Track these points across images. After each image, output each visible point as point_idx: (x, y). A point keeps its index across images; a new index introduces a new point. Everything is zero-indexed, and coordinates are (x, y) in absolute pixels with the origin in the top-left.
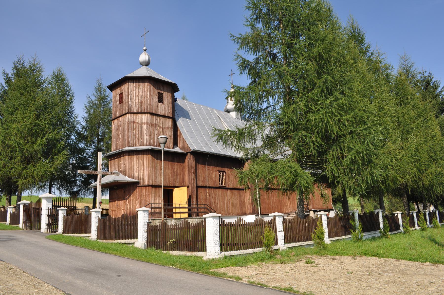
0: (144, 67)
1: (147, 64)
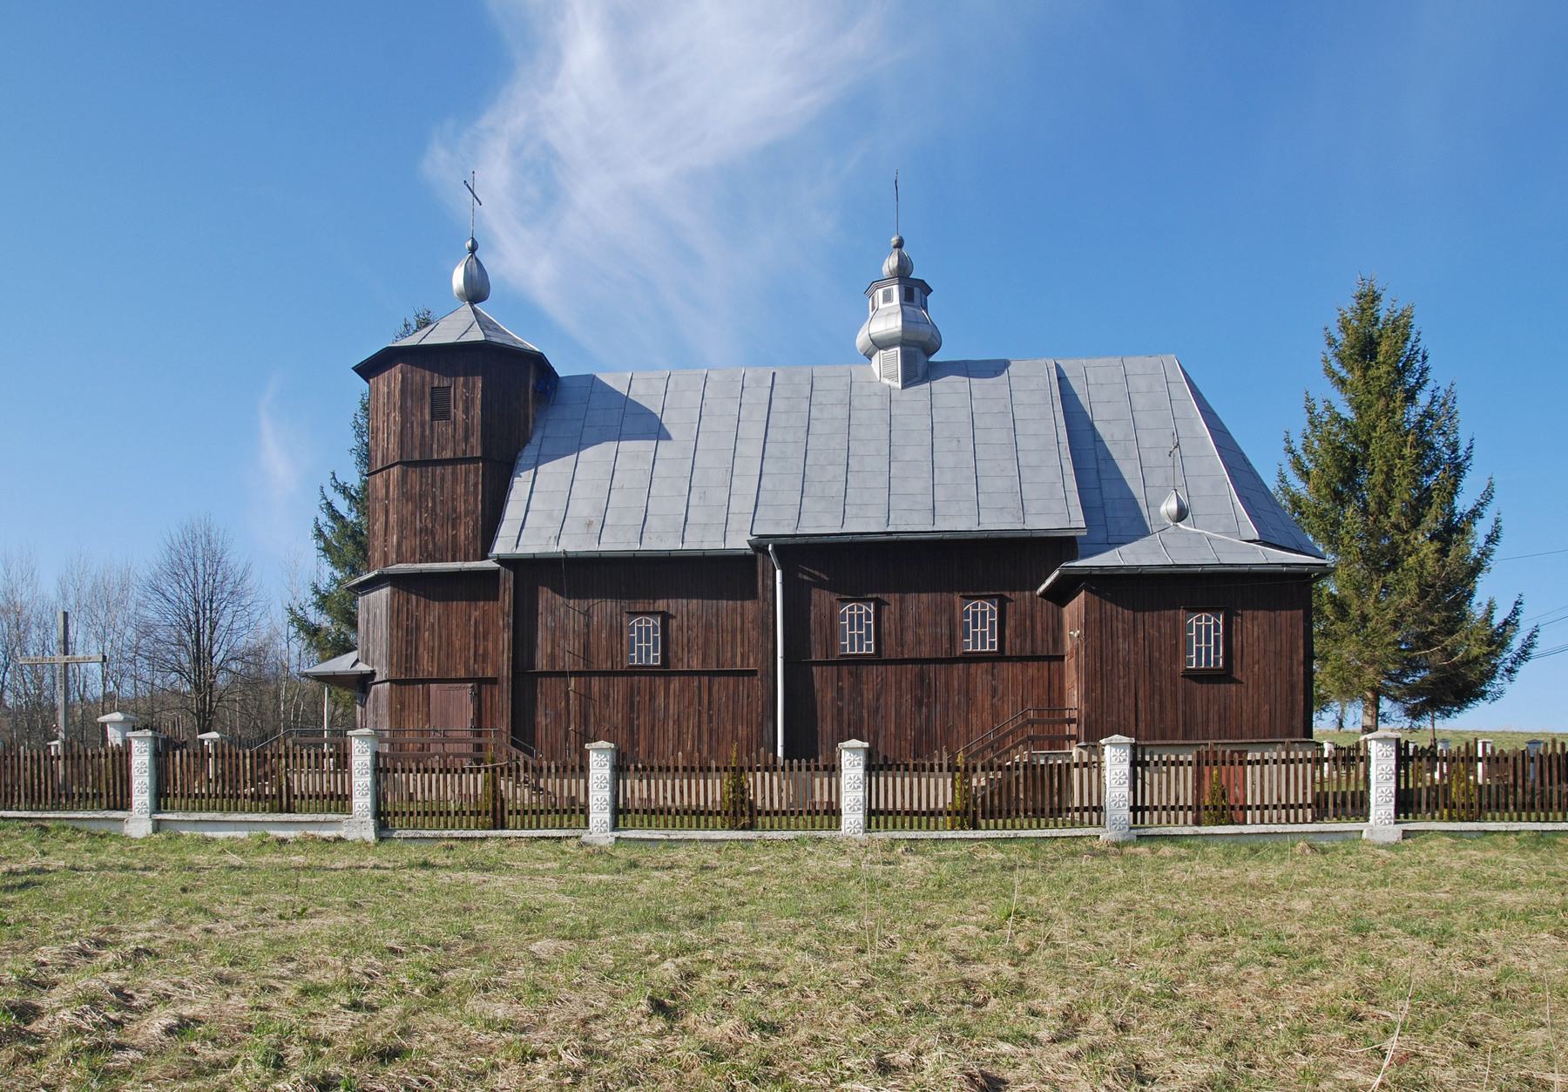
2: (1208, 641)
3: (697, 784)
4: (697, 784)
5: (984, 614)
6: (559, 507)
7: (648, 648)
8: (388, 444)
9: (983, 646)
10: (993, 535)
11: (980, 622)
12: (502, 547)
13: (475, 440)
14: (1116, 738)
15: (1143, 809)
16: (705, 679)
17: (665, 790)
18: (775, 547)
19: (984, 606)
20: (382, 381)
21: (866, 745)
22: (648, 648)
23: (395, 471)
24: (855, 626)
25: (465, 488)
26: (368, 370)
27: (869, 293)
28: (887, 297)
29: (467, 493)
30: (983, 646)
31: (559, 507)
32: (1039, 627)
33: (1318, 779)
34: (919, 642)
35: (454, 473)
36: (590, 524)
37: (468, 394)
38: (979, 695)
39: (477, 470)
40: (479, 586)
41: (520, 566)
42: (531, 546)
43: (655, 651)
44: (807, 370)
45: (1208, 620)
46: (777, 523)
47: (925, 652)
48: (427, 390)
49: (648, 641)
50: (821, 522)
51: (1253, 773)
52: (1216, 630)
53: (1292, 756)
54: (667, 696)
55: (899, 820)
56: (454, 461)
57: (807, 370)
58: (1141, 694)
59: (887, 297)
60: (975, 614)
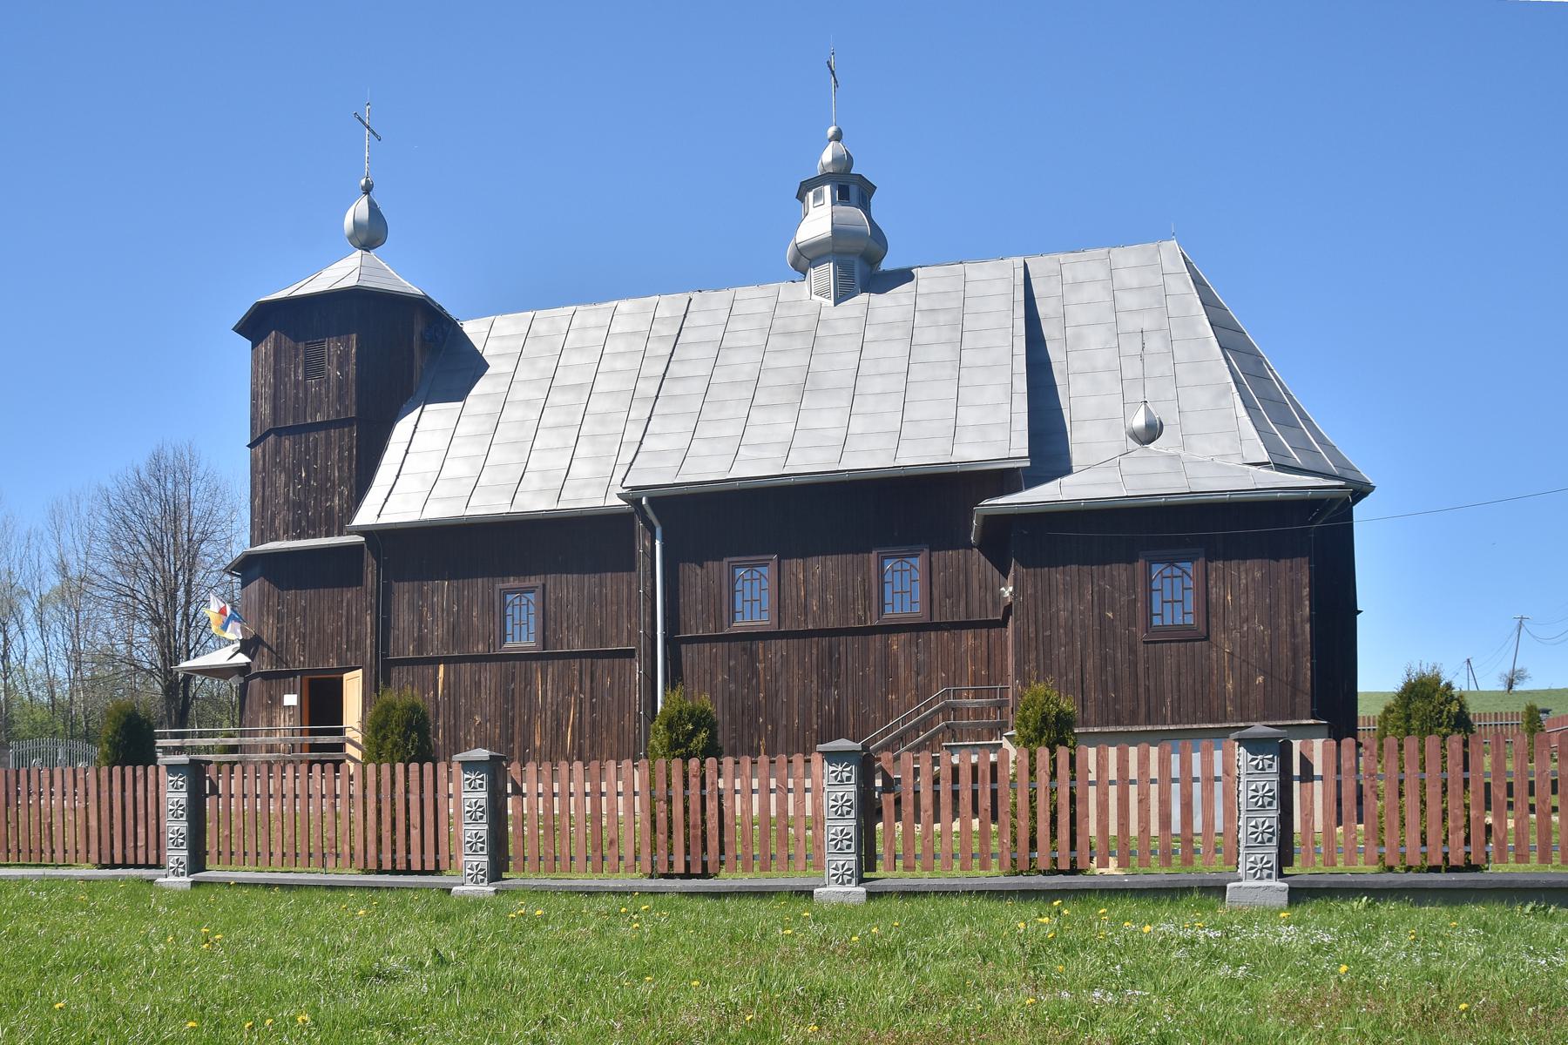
3: (1144, 829)
4: (1144, 829)
6: (431, 470)
10: (959, 469)
11: (904, 585)
12: (366, 515)
16: (587, 662)
18: (650, 500)
23: (271, 438)
24: (754, 595)
25: (336, 452)
27: (801, 197)
29: (341, 459)
31: (431, 470)
32: (975, 585)
34: (824, 607)
35: (328, 437)
37: (339, 355)
38: (901, 670)
39: (351, 432)
41: (381, 537)
44: (1019, 261)
47: (832, 622)
50: (710, 466)
54: (544, 682)
56: (325, 426)
57: (1019, 261)
58: (1089, 665)
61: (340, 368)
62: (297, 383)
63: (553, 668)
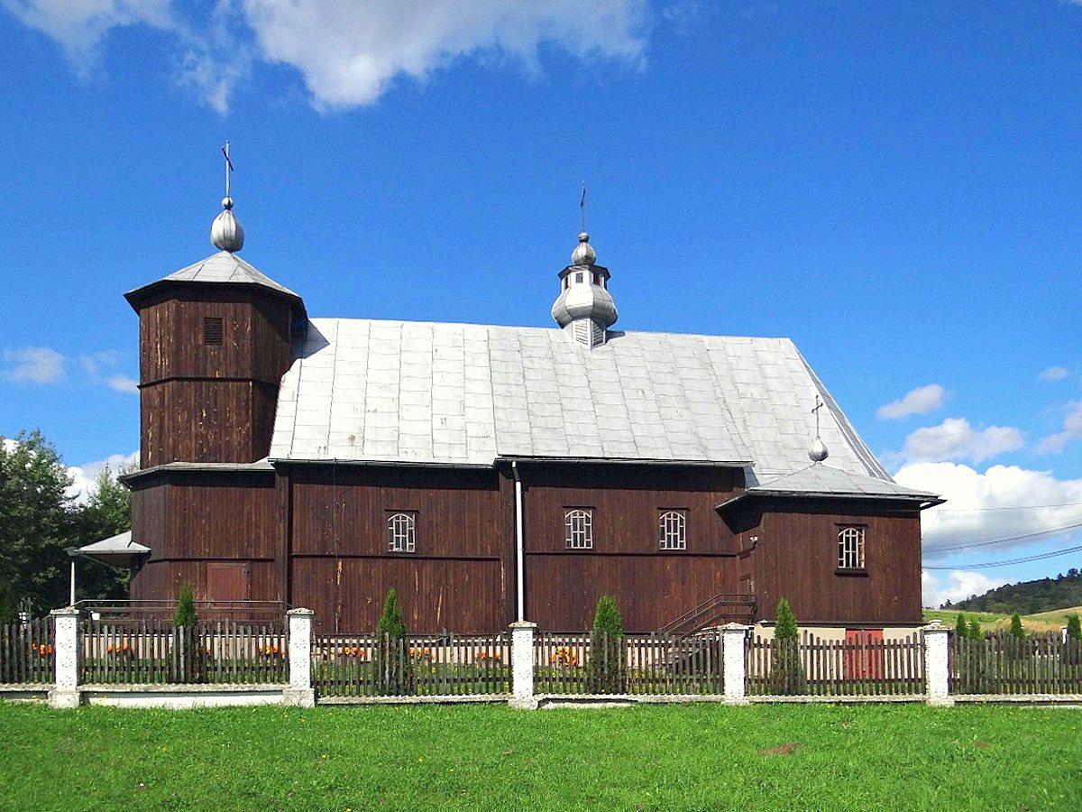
0: (225, 253)
1: (232, 245)
2: (854, 549)
5: (675, 522)
7: (675, 537)
8: (163, 363)
9: (675, 546)
13: (247, 363)
14: (732, 626)
15: (540, 680)
17: (877, 657)
19: (404, 518)
20: (155, 313)
21: (534, 625)
22: (675, 537)
24: (578, 526)
26: (141, 299)
27: (564, 274)
28: (580, 279)
29: (238, 407)
30: (675, 546)
33: (650, 662)
36: (353, 438)
40: (263, 479)
41: (285, 468)
42: (305, 451)
43: (411, 541)
45: (854, 533)
46: (518, 446)
48: (201, 319)
49: (675, 531)
51: (633, 653)
52: (860, 541)
53: (325, 641)
55: (491, 684)
59: (580, 279)
60: (398, 524)
61: (237, 339)
62: (197, 347)
63: (428, 567)
